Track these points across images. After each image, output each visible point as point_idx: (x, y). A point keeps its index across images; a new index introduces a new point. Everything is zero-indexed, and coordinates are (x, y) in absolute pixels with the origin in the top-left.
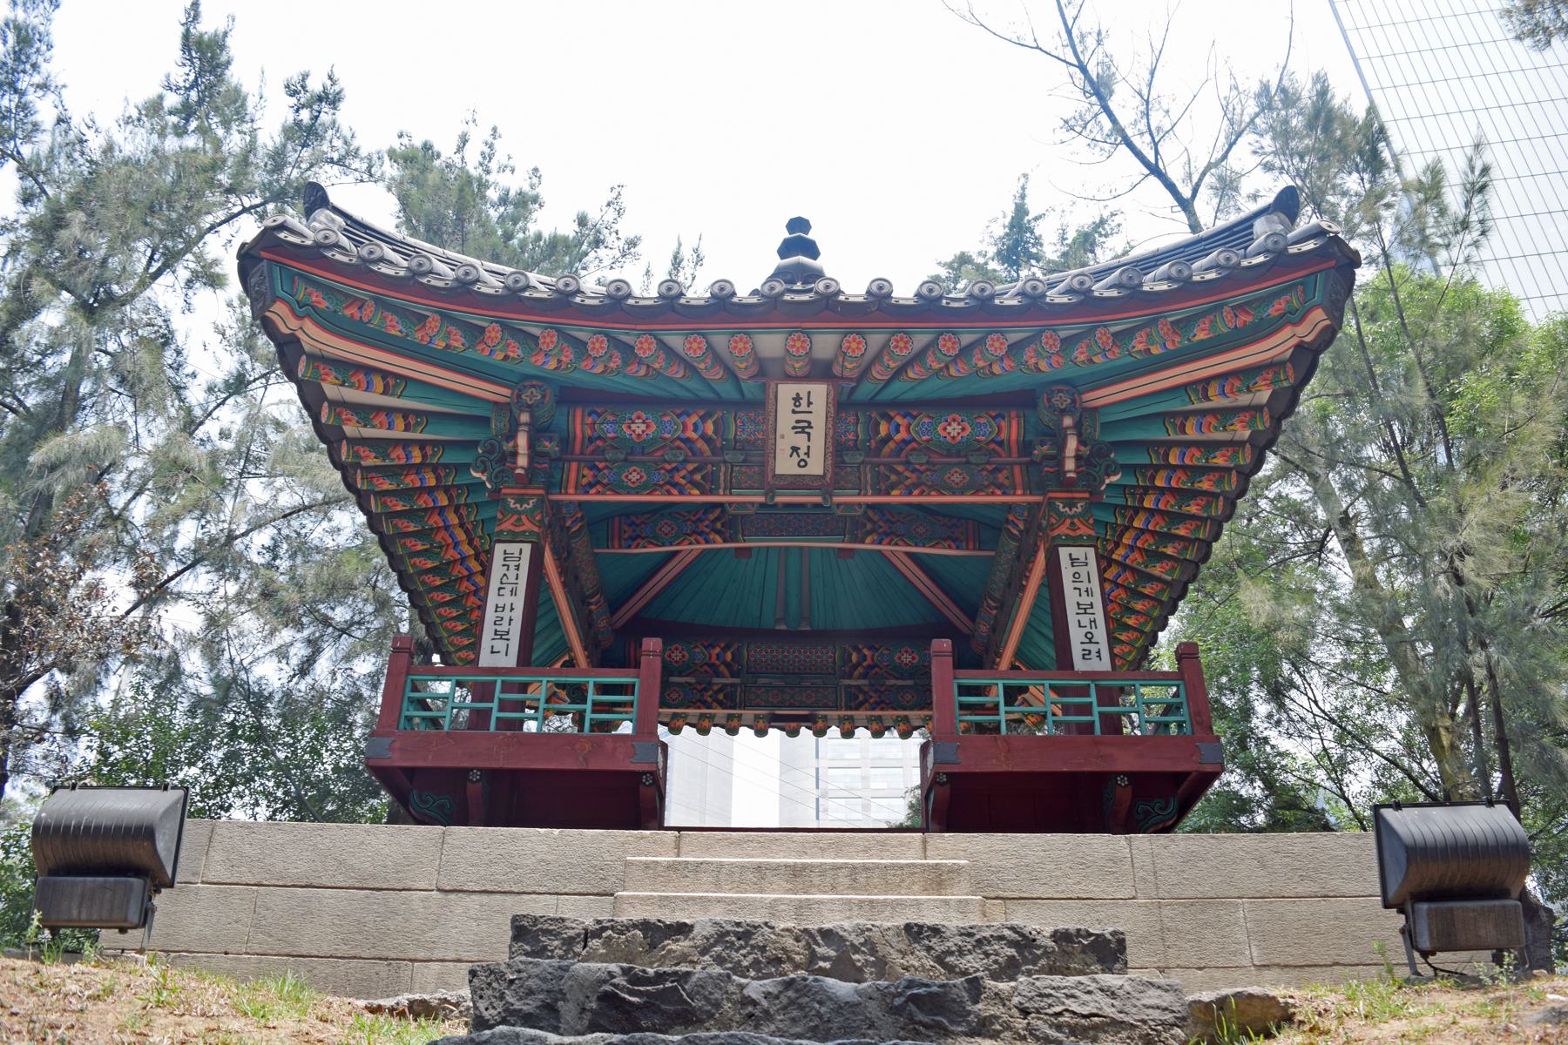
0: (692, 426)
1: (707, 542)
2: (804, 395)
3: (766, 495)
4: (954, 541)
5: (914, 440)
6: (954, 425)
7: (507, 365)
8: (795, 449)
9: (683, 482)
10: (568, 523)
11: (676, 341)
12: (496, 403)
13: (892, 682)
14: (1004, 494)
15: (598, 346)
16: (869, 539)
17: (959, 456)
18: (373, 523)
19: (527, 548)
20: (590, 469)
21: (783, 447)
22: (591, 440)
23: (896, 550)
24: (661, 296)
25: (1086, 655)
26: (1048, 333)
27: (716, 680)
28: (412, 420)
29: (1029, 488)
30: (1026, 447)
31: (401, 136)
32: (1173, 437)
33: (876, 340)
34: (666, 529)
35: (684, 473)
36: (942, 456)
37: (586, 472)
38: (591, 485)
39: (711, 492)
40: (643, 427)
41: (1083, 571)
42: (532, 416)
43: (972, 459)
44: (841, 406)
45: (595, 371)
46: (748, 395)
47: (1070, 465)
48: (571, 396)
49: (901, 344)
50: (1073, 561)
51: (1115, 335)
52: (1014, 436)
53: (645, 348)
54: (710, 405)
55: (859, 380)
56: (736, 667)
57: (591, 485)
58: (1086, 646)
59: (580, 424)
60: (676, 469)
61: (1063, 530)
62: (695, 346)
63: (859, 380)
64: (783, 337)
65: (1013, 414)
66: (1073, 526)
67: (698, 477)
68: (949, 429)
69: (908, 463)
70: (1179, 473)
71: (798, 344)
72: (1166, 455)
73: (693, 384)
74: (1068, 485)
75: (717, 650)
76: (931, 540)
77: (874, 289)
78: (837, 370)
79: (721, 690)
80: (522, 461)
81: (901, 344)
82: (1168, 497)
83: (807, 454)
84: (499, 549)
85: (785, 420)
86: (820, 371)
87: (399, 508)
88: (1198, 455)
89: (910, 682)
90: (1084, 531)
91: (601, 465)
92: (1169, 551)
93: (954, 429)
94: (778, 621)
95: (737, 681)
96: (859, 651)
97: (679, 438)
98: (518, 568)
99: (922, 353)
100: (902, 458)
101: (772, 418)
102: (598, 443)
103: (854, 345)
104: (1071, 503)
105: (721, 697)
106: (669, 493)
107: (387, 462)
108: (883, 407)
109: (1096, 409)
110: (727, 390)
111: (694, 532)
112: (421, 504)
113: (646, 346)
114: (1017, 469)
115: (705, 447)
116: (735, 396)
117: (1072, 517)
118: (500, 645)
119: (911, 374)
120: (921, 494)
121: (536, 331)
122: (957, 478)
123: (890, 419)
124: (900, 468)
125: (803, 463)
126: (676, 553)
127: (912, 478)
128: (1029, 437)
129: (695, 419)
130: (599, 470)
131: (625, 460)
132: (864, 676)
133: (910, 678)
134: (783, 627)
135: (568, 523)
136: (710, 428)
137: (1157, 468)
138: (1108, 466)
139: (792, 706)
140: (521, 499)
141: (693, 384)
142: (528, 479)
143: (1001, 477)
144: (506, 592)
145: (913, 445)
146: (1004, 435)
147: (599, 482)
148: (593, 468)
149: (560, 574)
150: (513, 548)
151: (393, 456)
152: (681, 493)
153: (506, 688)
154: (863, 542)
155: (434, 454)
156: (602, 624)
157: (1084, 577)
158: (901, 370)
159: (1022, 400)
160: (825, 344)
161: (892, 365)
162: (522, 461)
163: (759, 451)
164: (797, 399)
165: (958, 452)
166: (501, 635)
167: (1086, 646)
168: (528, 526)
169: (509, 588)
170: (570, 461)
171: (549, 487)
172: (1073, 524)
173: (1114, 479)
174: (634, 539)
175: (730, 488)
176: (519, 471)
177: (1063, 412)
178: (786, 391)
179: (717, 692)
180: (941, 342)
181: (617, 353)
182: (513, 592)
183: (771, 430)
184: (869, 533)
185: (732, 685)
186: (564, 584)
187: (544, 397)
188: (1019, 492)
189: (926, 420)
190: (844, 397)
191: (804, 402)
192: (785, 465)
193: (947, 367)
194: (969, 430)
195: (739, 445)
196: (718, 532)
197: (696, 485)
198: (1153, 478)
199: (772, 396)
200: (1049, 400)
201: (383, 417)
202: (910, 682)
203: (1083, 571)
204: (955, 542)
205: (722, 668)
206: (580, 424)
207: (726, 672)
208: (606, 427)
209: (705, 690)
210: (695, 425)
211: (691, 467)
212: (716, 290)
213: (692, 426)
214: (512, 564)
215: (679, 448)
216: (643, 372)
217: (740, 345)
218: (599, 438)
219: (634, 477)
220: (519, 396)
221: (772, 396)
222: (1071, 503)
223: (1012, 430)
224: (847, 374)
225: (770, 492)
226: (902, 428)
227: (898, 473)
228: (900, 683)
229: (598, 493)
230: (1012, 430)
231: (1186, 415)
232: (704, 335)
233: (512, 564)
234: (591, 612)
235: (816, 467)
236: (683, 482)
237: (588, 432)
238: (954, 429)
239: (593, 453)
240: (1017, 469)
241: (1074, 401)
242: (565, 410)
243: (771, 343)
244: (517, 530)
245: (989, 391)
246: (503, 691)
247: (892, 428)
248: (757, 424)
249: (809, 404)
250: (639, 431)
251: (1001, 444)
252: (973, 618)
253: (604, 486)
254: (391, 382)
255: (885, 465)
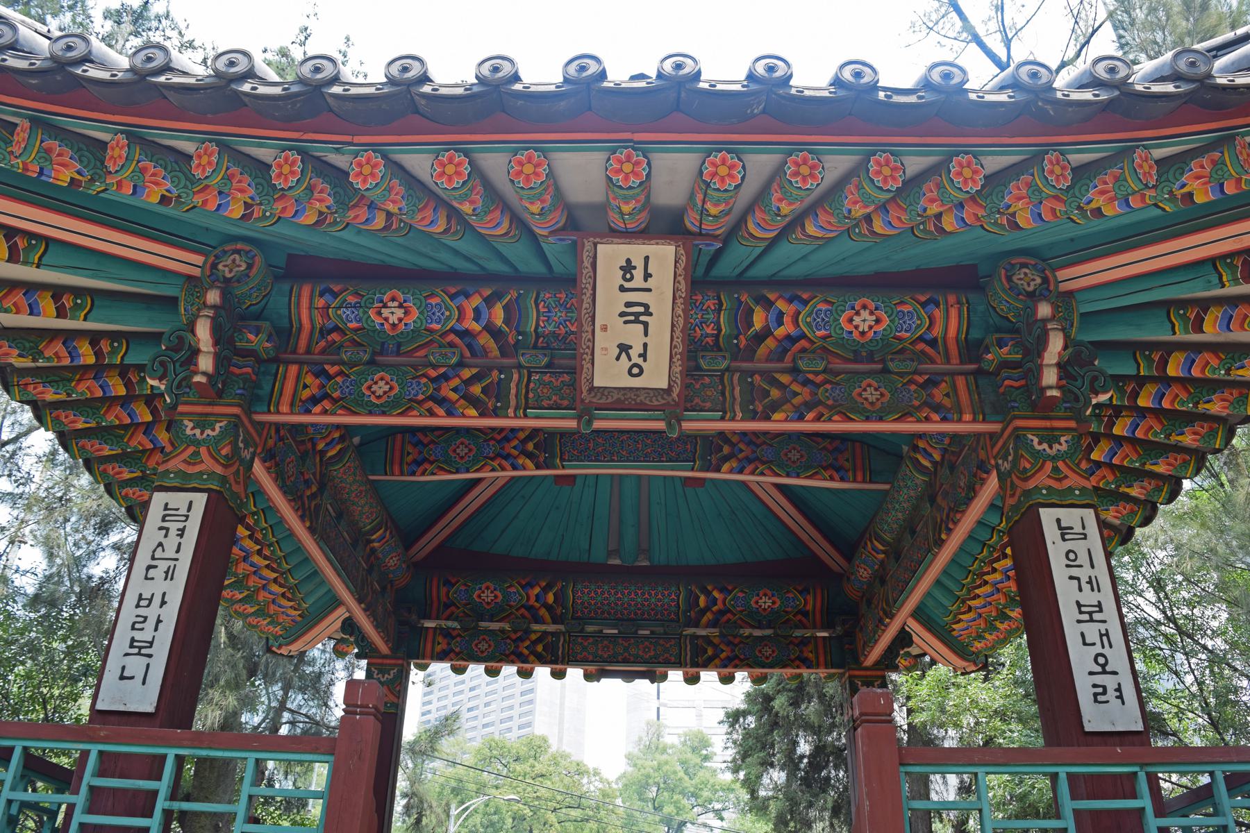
0: (473, 312)
1: (515, 468)
2: (638, 263)
3: (579, 418)
4: (837, 471)
5: (803, 336)
6: (865, 314)
7: (163, 210)
8: (624, 348)
9: (454, 396)
10: (321, 446)
11: (420, 163)
12: (190, 278)
13: (747, 632)
14: (944, 420)
15: (288, 171)
16: (725, 467)
17: (870, 359)
18: (64, 439)
19: (200, 500)
20: (317, 376)
21: (605, 344)
22: (324, 332)
23: (763, 481)
24: (391, 81)
25: (1099, 693)
26: (1052, 156)
27: (536, 627)
28: (68, 301)
29: (980, 413)
30: (972, 349)
31: (265, 51)
32: (1181, 336)
33: (760, 163)
34: (462, 451)
35: (456, 382)
36: (846, 360)
37: (309, 380)
38: (315, 400)
39: (495, 414)
40: (400, 313)
41: (1080, 547)
42: (224, 295)
43: (891, 366)
44: (699, 282)
45: (303, 221)
46: (558, 269)
47: (1050, 377)
48: (300, 268)
49: (805, 170)
50: (1064, 531)
51: (1160, 162)
52: (952, 332)
53: (367, 175)
54: (499, 282)
55: (727, 239)
56: (559, 611)
57: (315, 400)
58: (1099, 679)
59: (307, 307)
60: (446, 377)
61: (1042, 479)
62: (450, 169)
63: (727, 239)
64: (602, 156)
65: (952, 299)
66: (1057, 474)
67: (476, 389)
68: (857, 320)
69: (795, 371)
70: (1175, 389)
71: (627, 168)
72: (1164, 363)
73: (466, 246)
74: (1043, 407)
75: (537, 590)
76: (807, 468)
77: (760, 69)
78: (691, 222)
79: (539, 640)
80: (205, 363)
81: (805, 170)
82: (1150, 421)
83: (643, 356)
84: (159, 499)
85: (609, 301)
86: (665, 225)
87: (80, 426)
88: (1214, 362)
89: (768, 632)
90: (1073, 480)
91: (332, 370)
92: (1134, 492)
93: (864, 320)
94: (610, 554)
95: (562, 627)
96: (708, 594)
97: (452, 330)
98: (182, 532)
99: (839, 186)
100: (787, 364)
101: (587, 299)
102: (335, 336)
103: (723, 171)
104: (1050, 437)
105: (540, 648)
106: (432, 414)
107: (41, 363)
108: (761, 288)
109: (1070, 293)
110: (520, 255)
111: (499, 455)
112: (111, 419)
113: (367, 170)
114: (961, 381)
115: (492, 344)
116: (537, 268)
117: (1054, 458)
118: (136, 665)
119: (811, 229)
120: (818, 419)
121: (188, 147)
122: (871, 395)
123: (768, 304)
124: (785, 379)
125: (636, 371)
126: (480, 480)
127: (804, 394)
128: (975, 334)
129: (476, 301)
130: (330, 378)
131: (372, 362)
132: (713, 624)
133: (769, 627)
134: (617, 562)
135: (321, 446)
136: (498, 315)
137: (1141, 381)
138: (1095, 379)
139: (626, 661)
140: (203, 422)
141: (466, 246)
142: (217, 388)
143: (938, 394)
144: (158, 574)
145: (803, 343)
146: (937, 331)
147: (326, 396)
148: (320, 373)
149: (302, 518)
150: (179, 500)
151: (49, 353)
152: (450, 414)
153: (109, 765)
154: (718, 470)
155: (114, 352)
156: (392, 562)
157: (1083, 559)
158: (797, 222)
159: (962, 279)
160: (673, 173)
161: (785, 209)
162: (205, 363)
163: (566, 355)
164: (628, 268)
165: (876, 357)
166: (139, 648)
167: (1099, 679)
168: (208, 464)
169: (163, 566)
170: (288, 363)
171: (251, 401)
172: (1056, 469)
173: (1103, 398)
174: (419, 464)
175: (524, 407)
176: (198, 379)
177: (1034, 297)
178: (611, 255)
179: (535, 642)
180: (872, 167)
181: (320, 184)
182: (169, 575)
183: (585, 318)
184: (726, 459)
185: (553, 634)
186: (312, 530)
187: (250, 266)
188: (967, 417)
189: (824, 307)
190: (700, 271)
191: (638, 274)
192: (608, 373)
193: (868, 219)
194: (886, 321)
195: (541, 342)
196: (530, 456)
197: (473, 401)
198: (1135, 395)
199: (587, 263)
200: (1009, 279)
201: (18, 297)
202: (768, 632)
203: (1080, 547)
204: (838, 471)
205: (543, 612)
206: (307, 307)
207: (547, 617)
208: (345, 313)
209: (522, 640)
210: (477, 310)
211: (467, 373)
212: (486, 70)
213: (473, 312)
214: (174, 527)
215: (451, 345)
216: (379, 221)
217: (528, 169)
218: (336, 329)
219: (381, 388)
220: (214, 266)
221: (587, 263)
222: (1050, 437)
223: (950, 322)
224: (708, 226)
225: (585, 414)
226: (782, 319)
227: (782, 387)
228: (757, 633)
229: (325, 412)
230: (950, 322)
231: (1204, 305)
232: (467, 154)
233: (174, 527)
234: (373, 550)
235: (657, 376)
236: (454, 396)
237: (319, 321)
238: (864, 320)
239: (323, 352)
240: (961, 381)
241: (1045, 280)
242: (286, 287)
243: (582, 172)
244: (191, 470)
245: (910, 267)
246: (101, 772)
247: (772, 316)
248: (569, 310)
249: (647, 276)
250: (393, 319)
251: (933, 343)
252: (849, 558)
253: (335, 401)
254: (21, 243)
255: (762, 373)
